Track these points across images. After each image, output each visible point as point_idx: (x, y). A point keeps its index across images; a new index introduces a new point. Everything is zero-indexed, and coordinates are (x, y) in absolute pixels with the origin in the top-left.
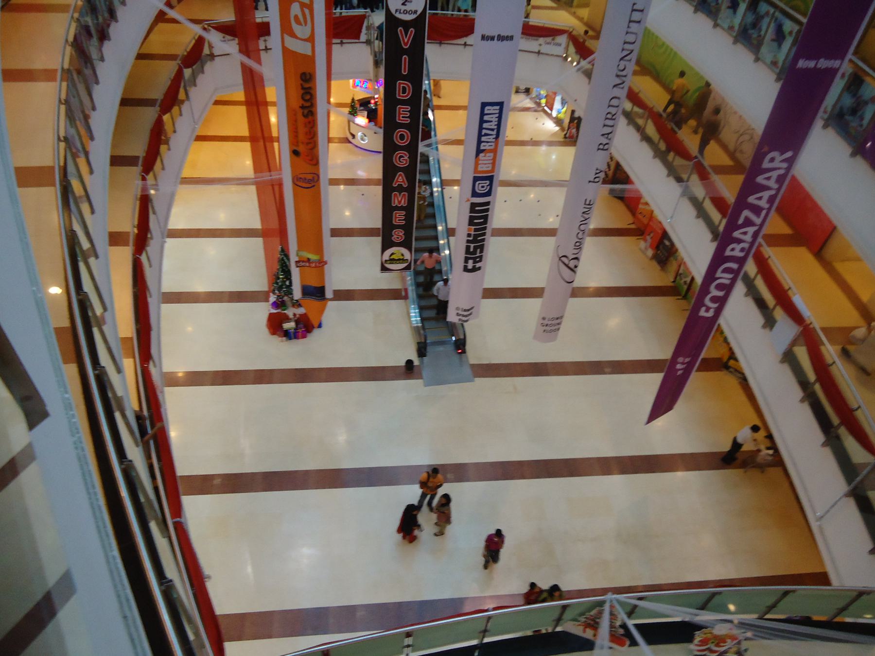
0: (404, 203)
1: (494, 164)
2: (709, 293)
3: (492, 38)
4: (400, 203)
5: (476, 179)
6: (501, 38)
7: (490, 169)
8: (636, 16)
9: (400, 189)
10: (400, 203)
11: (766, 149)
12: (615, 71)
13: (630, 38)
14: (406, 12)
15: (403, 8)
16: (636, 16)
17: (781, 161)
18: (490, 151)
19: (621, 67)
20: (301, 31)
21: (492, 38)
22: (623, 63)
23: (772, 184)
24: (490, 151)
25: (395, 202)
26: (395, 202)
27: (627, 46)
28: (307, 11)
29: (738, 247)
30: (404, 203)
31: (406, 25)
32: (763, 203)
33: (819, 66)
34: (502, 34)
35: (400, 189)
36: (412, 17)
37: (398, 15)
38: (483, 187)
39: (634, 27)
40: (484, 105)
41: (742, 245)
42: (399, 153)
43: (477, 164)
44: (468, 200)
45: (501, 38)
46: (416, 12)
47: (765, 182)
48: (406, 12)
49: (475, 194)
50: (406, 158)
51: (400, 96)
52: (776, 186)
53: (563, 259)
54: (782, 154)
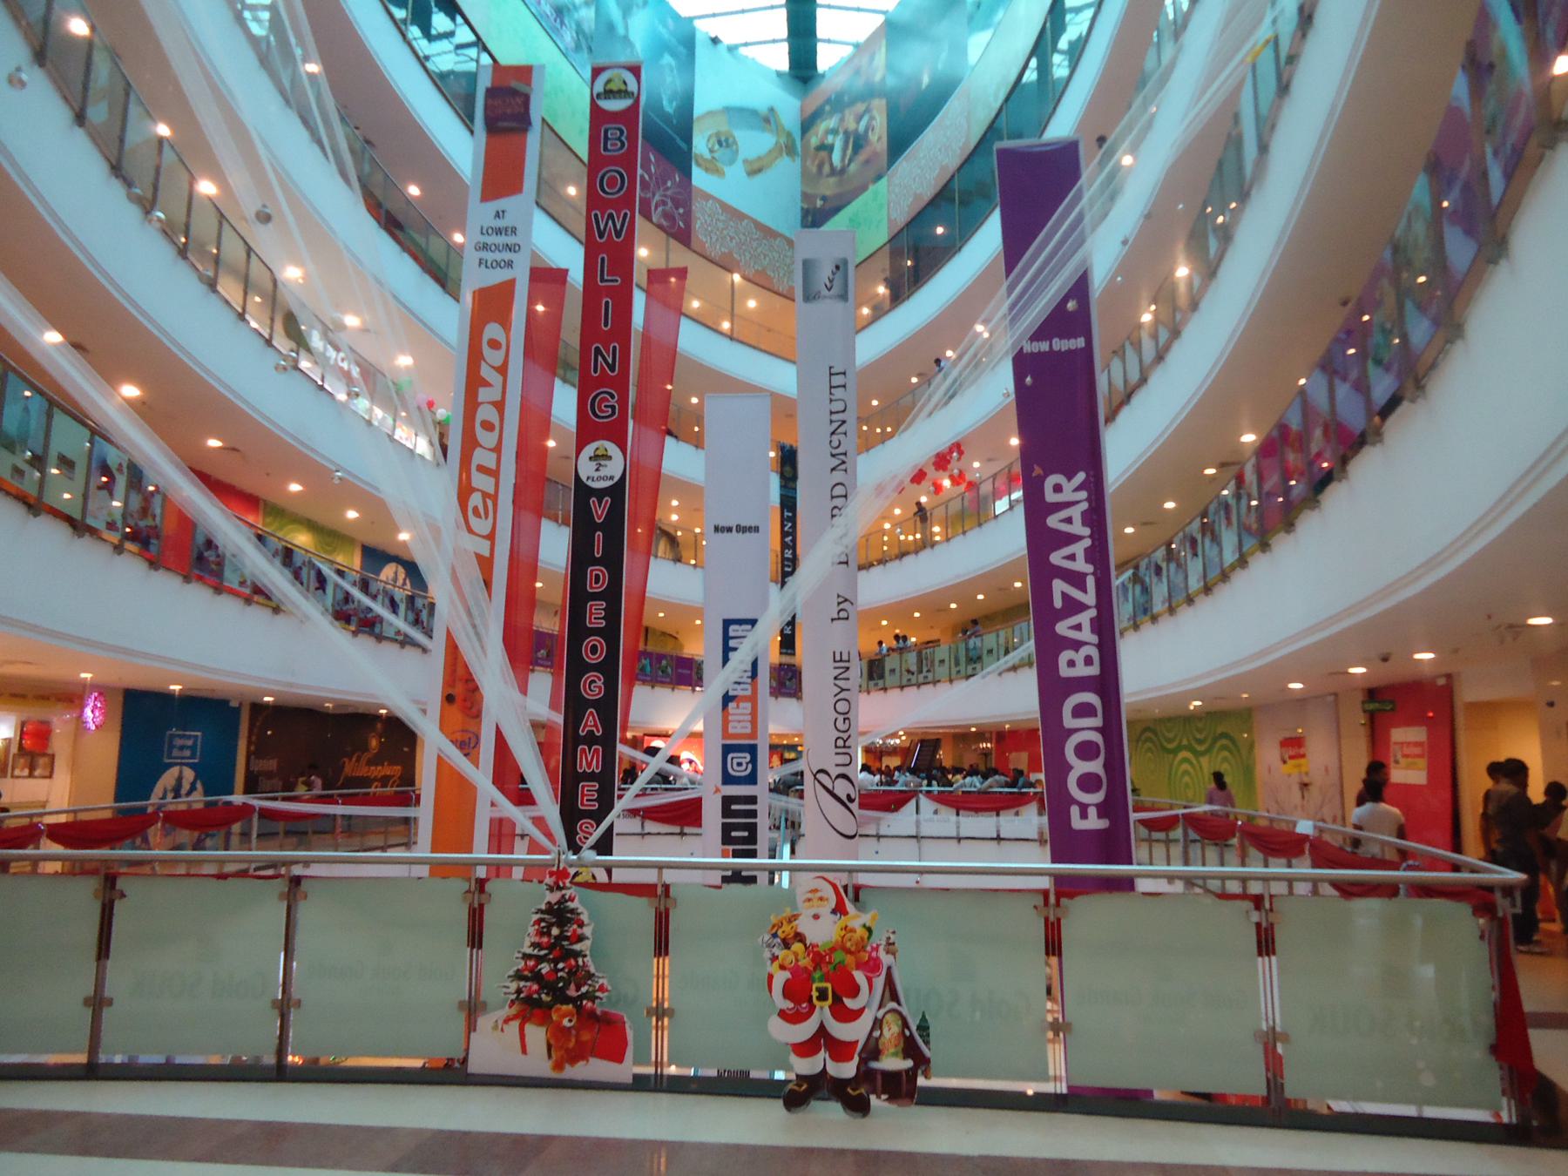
0: (596, 767)
1: (754, 722)
2: (1070, 768)
3: (729, 530)
4: (589, 765)
5: (727, 750)
6: (742, 529)
7: (748, 731)
8: (837, 380)
9: (591, 739)
10: (589, 765)
11: (1038, 471)
12: (829, 450)
13: (838, 406)
14: (600, 478)
15: (596, 474)
16: (837, 380)
17: (1077, 489)
18: (745, 699)
19: (835, 444)
20: (482, 526)
21: (729, 530)
22: (835, 438)
23: (1078, 528)
24: (745, 699)
25: (582, 767)
26: (582, 767)
27: (835, 417)
28: (490, 503)
29: (1079, 657)
30: (596, 767)
31: (600, 493)
32: (1081, 565)
33: (1056, 348)
34: (743, 524)
35: (591, 739)
36: (610, 483)
37: (590, 483)
38: (739, 764)
39: (838, 393)
40: (727, 623)
41: (1085, 651)
42: (591, 675)
43: (726, 722)
44: (717, 790)
45: (742, 529)
46: (612, 478)
47: (1064, 527)
48: (600, 478)
49: (728, 779)
50: (600, 683)
51: (592, 588)
52: (1086, 531)
53: (821, 776)
54: (1070, 479)
